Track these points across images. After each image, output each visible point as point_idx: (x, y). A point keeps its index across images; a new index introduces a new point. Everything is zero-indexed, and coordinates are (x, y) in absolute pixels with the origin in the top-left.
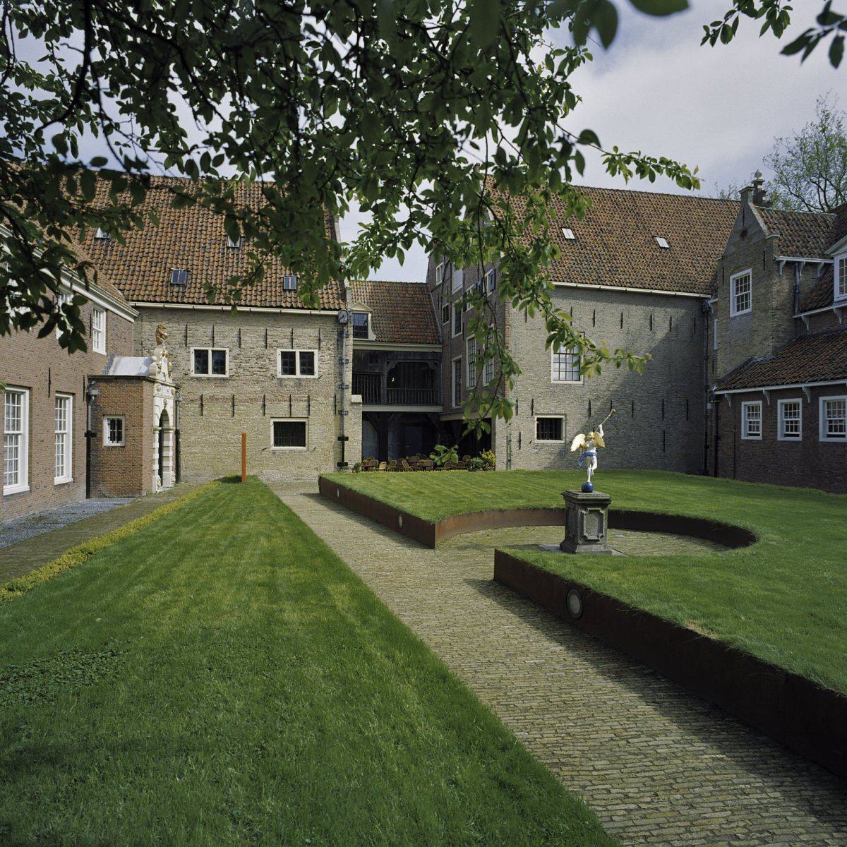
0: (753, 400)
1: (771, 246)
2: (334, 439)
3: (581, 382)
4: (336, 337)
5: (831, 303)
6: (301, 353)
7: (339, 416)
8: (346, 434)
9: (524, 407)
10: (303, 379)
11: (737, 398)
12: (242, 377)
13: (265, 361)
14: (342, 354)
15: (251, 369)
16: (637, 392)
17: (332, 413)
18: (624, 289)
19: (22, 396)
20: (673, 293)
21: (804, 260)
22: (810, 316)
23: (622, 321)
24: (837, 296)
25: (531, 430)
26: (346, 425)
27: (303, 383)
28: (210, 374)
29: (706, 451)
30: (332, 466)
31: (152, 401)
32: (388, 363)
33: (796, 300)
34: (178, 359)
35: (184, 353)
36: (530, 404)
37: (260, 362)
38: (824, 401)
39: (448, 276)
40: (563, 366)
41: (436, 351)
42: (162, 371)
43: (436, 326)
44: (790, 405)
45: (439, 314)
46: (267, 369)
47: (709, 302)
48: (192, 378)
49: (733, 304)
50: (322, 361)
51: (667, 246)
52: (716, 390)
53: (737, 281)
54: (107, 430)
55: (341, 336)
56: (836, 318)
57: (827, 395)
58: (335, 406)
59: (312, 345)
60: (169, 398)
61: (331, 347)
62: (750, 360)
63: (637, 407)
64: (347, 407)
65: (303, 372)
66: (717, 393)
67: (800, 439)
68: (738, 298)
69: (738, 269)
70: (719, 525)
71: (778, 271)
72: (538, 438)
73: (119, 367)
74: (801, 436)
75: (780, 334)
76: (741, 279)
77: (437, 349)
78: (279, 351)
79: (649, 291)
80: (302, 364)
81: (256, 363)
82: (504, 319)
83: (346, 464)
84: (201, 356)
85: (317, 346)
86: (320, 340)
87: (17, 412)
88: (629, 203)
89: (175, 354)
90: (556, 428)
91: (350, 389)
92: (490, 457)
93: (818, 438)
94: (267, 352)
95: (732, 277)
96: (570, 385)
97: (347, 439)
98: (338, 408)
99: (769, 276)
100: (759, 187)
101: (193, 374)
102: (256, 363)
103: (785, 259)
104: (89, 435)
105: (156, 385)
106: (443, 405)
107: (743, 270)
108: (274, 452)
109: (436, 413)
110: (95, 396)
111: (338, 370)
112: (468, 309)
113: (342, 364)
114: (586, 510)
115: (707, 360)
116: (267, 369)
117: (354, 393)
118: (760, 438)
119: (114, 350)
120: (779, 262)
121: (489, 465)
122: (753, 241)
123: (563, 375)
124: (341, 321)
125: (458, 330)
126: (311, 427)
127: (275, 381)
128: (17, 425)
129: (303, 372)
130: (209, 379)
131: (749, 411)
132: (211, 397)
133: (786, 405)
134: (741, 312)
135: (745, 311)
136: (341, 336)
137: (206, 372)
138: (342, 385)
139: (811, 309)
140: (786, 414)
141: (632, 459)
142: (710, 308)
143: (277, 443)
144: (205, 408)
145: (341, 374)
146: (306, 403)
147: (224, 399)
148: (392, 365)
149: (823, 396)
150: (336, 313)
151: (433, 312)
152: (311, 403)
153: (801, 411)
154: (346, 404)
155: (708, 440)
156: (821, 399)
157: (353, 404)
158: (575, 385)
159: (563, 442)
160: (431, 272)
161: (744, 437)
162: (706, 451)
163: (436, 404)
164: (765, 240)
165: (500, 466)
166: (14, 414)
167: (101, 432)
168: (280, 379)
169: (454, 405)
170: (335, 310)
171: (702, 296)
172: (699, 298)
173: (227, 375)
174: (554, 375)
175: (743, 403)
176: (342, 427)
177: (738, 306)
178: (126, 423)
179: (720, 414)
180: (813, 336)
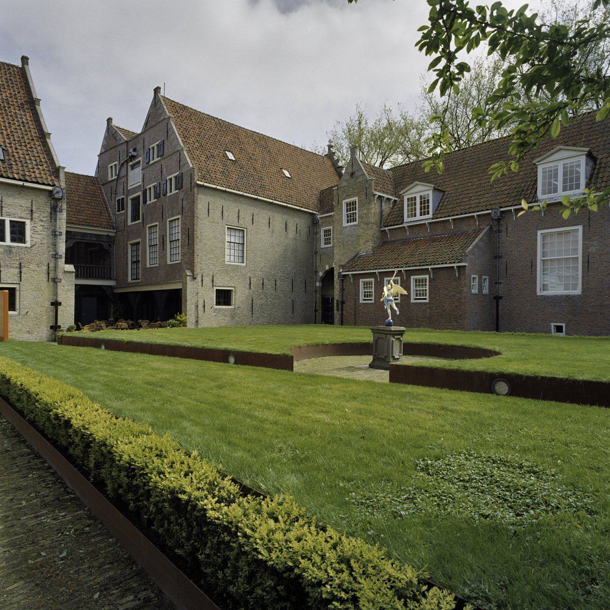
0: (368, 278)
1: (370, 185)
2: (48, 304)
3: (244, 264)
4: (49, 210)
5: (402, 223)
6: (11, 221)
7: (52, 284)
8: (59, 300)
9: (207, 280)
10: (14, 247)
11: (357, 277)
14: (55, 226)
17: (45, 280)
18: (271, 201)
20: (299, 208)
22: (390, 230)
23: (269, 223)
24: (406, 219)
25: (212, 298)
26: (59, 291)
27: (14, 250)
29: (316, 313)
30: (45, 329)
33: (383, 221)
36: (211, 278)
38: (414, 279)
39: (123, 173)
40: (232, 251)
41: (111, 234)
43: (109, 214)
44: (367, 282)
45: (113, 205)
47: (318, 217)
49: (345, 218)
50: (33, 229)
52: (342, 272)
53: (347, 204)
55: (54, 210)
56: (406, 231)
57: (415, 275)
58: (48, 274)
59: (24, 215)
61: (44, 219)
62: (358, 254)
64: (60, 276)
65: (13, 240)
66: (343, 273)
67: (373, 302)
69: (349, 196)
70: (440, 346)
72: (216, 305)
74: (399, 300)
76: (350, 203)
79: (286, 205)
80: (12, 232)
82: (193, 212)
83: (60, 327)
85: (29, 216)
86: (32, 211)
88: (263, 142)
90: (228, 296)
91: (64, 259)
92: (183, 319)
93: (410, 301)
95: (344, 201)
96: (238, 266)
97: (60, 304)
98: (51, 276)
99: (369, 203)
100: (331, 149)
106: (116, 280)
107: (352, 197)
109: (110, 287)
111: (51, 241)
112: (148, 202)
113: (56, 235)
114: (394, 338)
115: (316, 254)
117: (66, 262)
118: (373, 302)
120: (374, 195)
121: (183, 324)
122: (359, 180)
123: (232, 258)
124: (56, 196)
125: (135, 217)
126: (22, 293)
129: (13, 240)
131: (364, 285)
133: (416, 280)
134: (350, 224)
135: (352, 224)
136: (54, 210)
138: (56, 254)
139: (391, 226)
140: (364, 287)
141: (275, 319)
142: (318, 221)
145: (55, 245)
146: (18, 270)
149: (413, 275)
150: (50, 188)
151: (105, 202)
152: (24, 270)
153: (428, 283)
154: (60, 271)
155: (317, 306)
156: (412, 277)
157: (65, 272)
158: (240, 266)
159: (233, 307)
160: (101, 167)
161: (361, 301)
162: (316, 313)
163: (110, 279)
164: (367, 181)
165: (190, 324)
169: (130, 279)
170: (49, 185)
171: (314, 212)
172: (312, 213)
174: (227, 258)
175: (361, 280)
176: (56, 294)
177: (348, 220)
179: (344, 287)
180: (392, 241)
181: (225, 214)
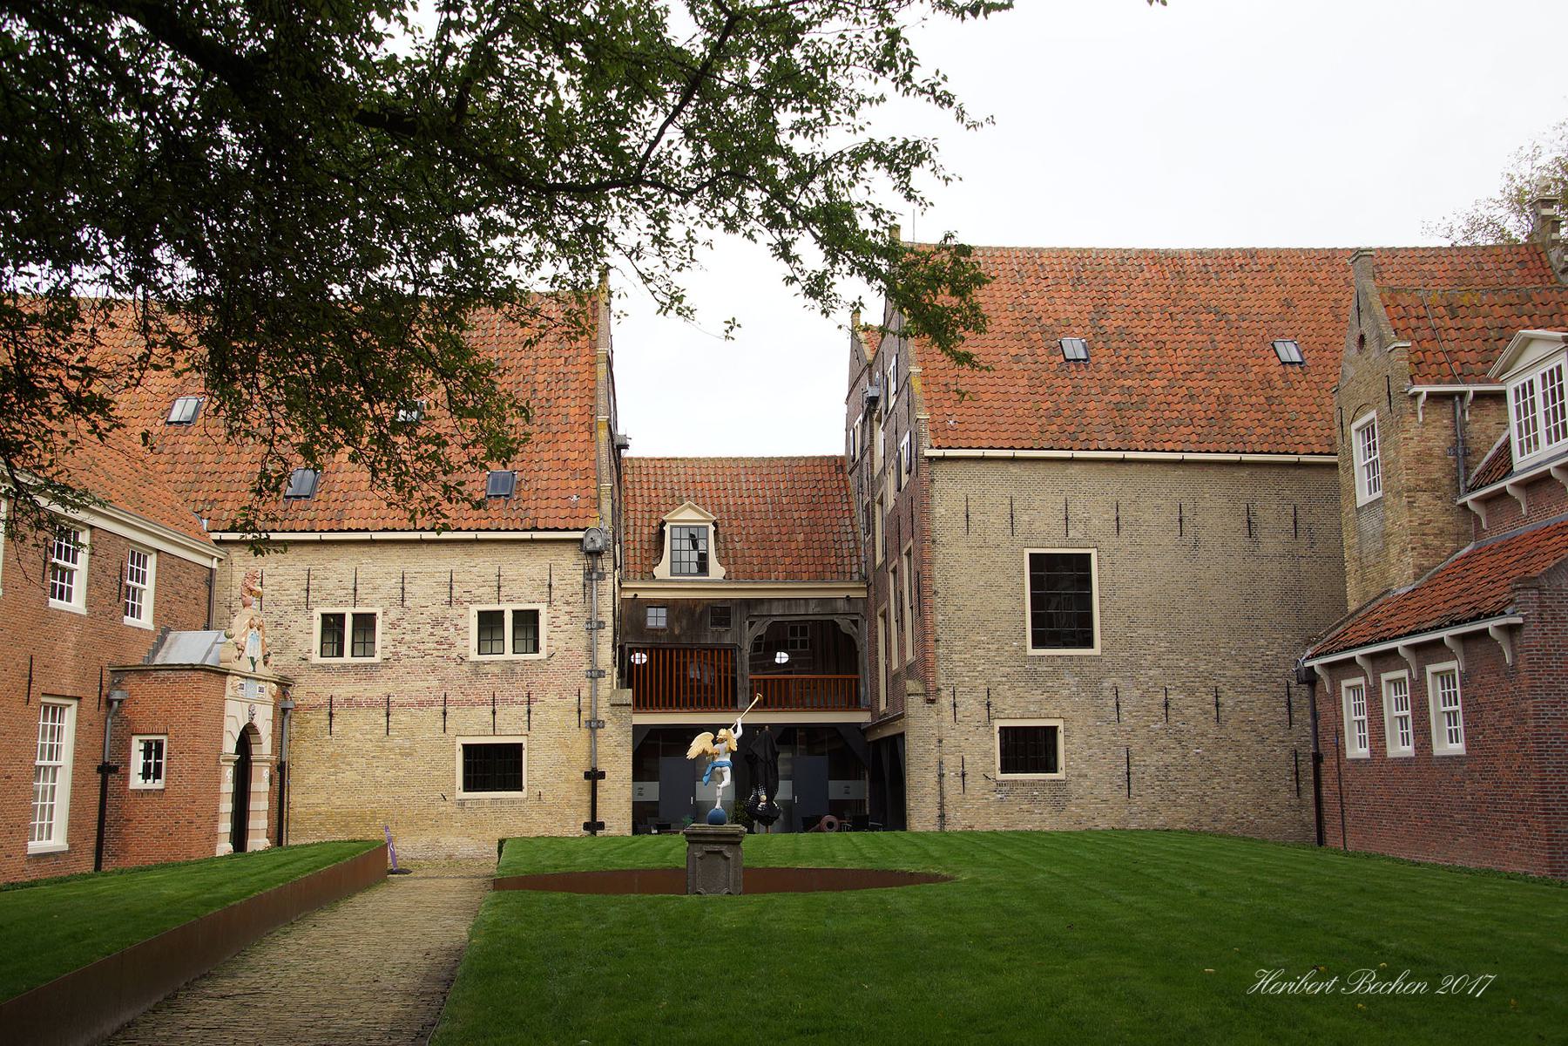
4: (581, 579)
7: (585, 732)
8: (601, 768)
12: (405, 661)
13: (446, 629)
15: (421, 647)
16: (1224, 668)
19: (67, 710)
21: (1471, 389)
26: (601, 748)
27: (518, 669)
28: (347, 658)
31: (222, 709)
32: (751, 624)
34: (292, 631)
35: (303, 621)
37: (439, 632)
41: (853, 595)
42: (248, 653)
46: (452, 645)
48: (313, 666)
51: (1296, 358)
54: (137, 761)
60: (264, 702)
63: (1228, 700)
68: (1368, 465)
71: (1415, 414)
73: (173, 651)
75: (1430, 540)
77: (838, 591)
78: (474, 610)
81: (432, 634)
84: (332, 624)
87: (55, 733)
89: (286, 623)
94: (451, 612)
97: (602, 775)
101: (316, 659)
102: (432, 634)
103: (1424, 389)
104: (106, 770)
105: (229, 679)
108: (462, 803)
110: (120, 701)
116: (452, 645)
119: (168, 623)
120: (1415, 396)
124: (590, 547)
127: (465, 667)
128: (53, 752)
130: (344, 666)
132: (347, 700)
137: (340, 654)
141: (1222, 811)
143: (468, 786)
144: (336, 720)
147: (372, 705)
148: (761, 629)
150: (579, 535)
166: (52, 735)
167: (127, 764)
168: (477, 664)
173: (377, 659)
178: (169, 748)
181: (1023, 518)
